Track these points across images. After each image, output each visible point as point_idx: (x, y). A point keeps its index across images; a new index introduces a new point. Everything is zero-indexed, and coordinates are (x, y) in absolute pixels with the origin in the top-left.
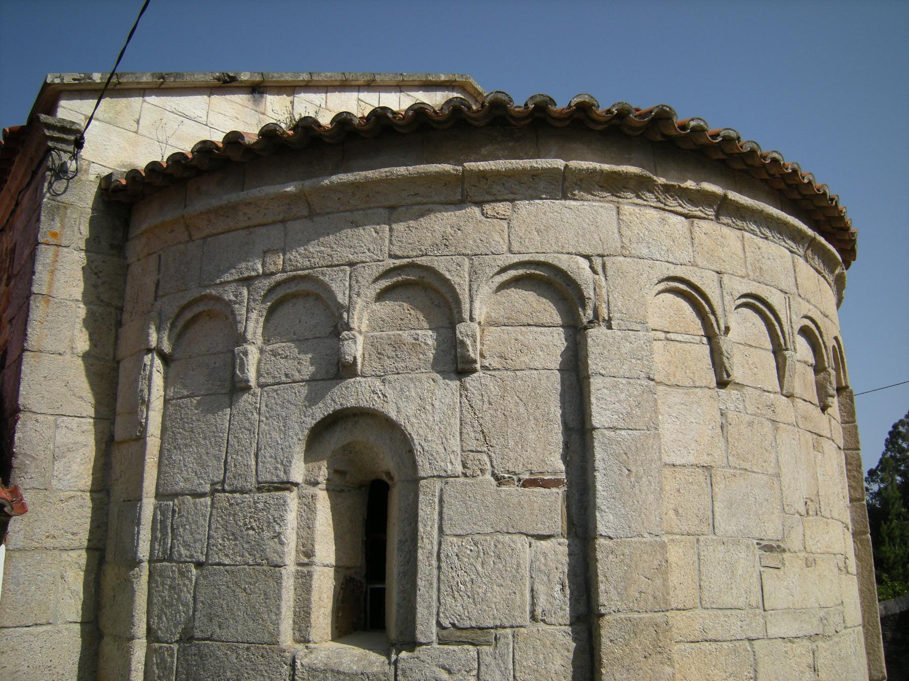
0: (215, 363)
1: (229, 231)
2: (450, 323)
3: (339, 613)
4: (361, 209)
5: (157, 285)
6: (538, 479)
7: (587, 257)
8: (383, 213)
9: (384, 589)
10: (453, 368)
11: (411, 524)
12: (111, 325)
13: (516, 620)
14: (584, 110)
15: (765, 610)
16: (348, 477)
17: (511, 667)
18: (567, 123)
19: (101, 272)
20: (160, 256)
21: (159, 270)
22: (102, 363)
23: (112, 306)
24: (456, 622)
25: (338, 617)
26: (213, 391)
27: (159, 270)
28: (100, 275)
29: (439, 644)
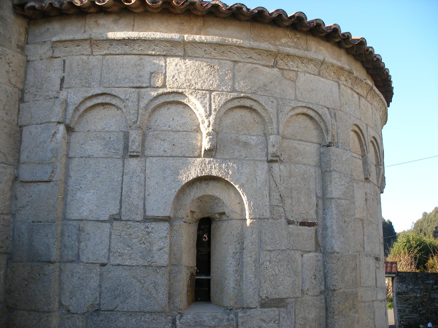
0: (110, 138)
1: (124, 54)
2: (264, 133)
3: (429, 279)
4: (217, 59)
5: (62, 80)
6: (306, 222)
7: (328, 108)
8: (230, 64)
9: (209, 280)
10: (266, 159)
11: (239, 243)
12: (16, 101)
13: (296, 294)
14: (335, 30)
15: (377, 287)
16: (195, 215)
17: (294, 317)
18: (160, 10)
19: (12, 63)
20: (64, 61)
21: (64, 70)
22: (11, 126)
23: (17, 87)
24: (269, 296)
25: (188, 295)
26: (109, 156)
27: (64, 70)
28: (11, 65)
29: (261, 308)
